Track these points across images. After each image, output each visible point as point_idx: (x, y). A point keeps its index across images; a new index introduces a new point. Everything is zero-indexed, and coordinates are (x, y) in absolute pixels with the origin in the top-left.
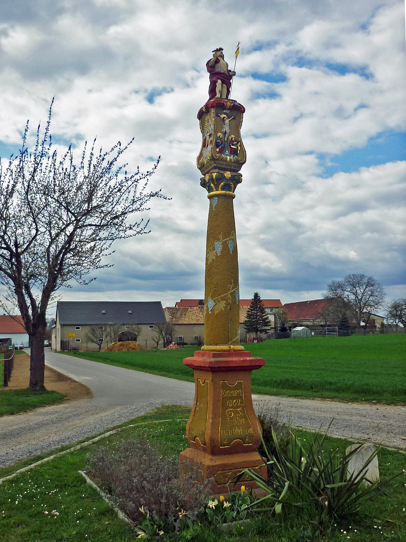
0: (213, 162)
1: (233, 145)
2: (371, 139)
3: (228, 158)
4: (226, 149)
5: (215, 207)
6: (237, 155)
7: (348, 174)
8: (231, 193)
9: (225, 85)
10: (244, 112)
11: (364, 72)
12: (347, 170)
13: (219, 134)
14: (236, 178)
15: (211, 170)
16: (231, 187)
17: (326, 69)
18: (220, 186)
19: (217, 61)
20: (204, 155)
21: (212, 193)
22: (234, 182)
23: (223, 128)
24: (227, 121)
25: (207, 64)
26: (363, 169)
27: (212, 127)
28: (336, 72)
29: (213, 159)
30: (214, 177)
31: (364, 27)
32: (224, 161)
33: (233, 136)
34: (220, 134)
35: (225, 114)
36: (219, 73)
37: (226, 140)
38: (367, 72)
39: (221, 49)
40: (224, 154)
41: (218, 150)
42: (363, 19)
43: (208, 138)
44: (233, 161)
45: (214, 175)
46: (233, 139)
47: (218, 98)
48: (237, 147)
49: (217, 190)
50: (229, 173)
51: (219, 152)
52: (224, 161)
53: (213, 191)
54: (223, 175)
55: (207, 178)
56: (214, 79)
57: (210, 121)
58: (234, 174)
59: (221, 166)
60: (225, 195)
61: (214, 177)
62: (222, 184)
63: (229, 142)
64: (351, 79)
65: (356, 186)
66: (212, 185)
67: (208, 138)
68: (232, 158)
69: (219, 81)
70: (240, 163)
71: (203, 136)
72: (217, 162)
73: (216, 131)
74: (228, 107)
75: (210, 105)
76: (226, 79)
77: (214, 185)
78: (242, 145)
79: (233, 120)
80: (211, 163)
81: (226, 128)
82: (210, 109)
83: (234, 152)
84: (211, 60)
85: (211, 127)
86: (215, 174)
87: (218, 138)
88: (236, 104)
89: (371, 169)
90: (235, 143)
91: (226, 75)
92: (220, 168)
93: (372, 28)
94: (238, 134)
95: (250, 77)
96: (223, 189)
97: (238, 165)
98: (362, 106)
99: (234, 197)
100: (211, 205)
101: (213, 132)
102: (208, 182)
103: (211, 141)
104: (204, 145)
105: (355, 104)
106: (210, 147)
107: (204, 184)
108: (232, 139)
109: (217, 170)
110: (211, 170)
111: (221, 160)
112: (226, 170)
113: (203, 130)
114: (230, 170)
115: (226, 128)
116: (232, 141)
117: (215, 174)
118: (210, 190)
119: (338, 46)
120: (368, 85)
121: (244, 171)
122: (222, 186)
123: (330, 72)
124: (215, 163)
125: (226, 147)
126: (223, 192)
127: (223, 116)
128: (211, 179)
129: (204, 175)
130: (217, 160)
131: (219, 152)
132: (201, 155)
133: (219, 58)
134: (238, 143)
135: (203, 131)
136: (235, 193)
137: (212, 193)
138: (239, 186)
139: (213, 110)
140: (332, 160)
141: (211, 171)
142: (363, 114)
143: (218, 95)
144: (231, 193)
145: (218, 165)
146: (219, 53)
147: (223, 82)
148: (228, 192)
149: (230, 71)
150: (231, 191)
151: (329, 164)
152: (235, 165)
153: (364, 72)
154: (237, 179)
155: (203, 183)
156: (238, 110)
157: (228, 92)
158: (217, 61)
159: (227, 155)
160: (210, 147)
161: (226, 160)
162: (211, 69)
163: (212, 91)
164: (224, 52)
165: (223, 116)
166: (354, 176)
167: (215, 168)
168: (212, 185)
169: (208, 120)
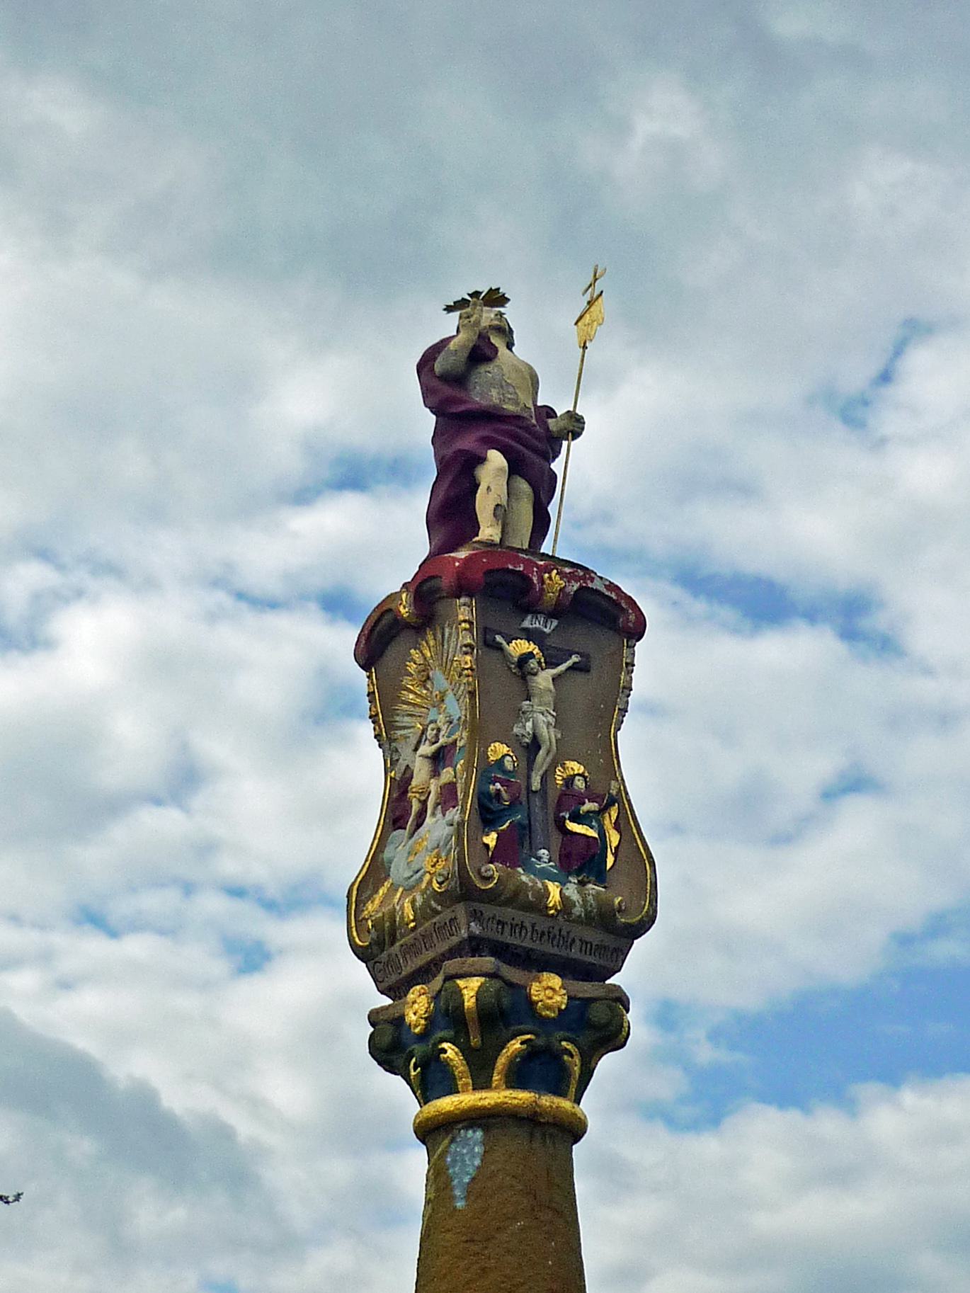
0: (461, 911)
1: (576, 818)
2: (905, 940)
3: (554, 890)
4: (539, 838)
5: (470, 1192)
6: (600, 876)
7: (793, 1116)
8: (566, 1104)
9: (523, 486)
10: (637, 630)
11: (852, 616)
12: (787, 1094)
13: (498, 750)
14: (598, 1013)
15: (453, 953)
16: (564, 1071)
17: (676, 592)
18: (502, 1061)
19: (481, 353)
20: (399, 870)
21: (447, 1104)
22: (587, 1037)
23: (519, 715)
24: (544, 679)
25: (425, 365)
26: (867, 1091)
27: (455, 708)
28: (727, 613)
29: (463, 890)
30: (469, 1002)
31: (852, 412)
32: (530, 907)
33: (575, 767)
34: (504, 749)
35: (530, 635)
36: (491, 416)
37: (536, 784)
38: (865, 623)
39: (496, 298)
40: (529, 869)
41: (491, 840)
42: (855, 374)
43: (421, 771)
44: (578, 910)
45: (470, 988)
46: (579, 784)
47: (490, 544)
48: (602, 833)
49: (482, 1084)
50: (556, 981)
51: (497, 855)
52: (530, 907)
53: (453, 1090)
54: (520, 991)
55: (417, 1006)
56: (467, 442)
57: (437, 674)
58: (587, 989)
59: (508, 939)
60: (529, 1120)
61: (469, 1002)
62: (515, 1045)
63: (553, 797)
64: (793, 654)
65: (841, 1175)
66: (451, 1052)
67: (421, 771)
68: (572, 891)
69: (496, 459)
70: (621, 929)
71: (391, 762)
72: (489, 910)
73: (480, 732)
74: (551, 596)
75: (446, 582)
76: (535, 450)
77: (466, 1051)
78: (627, 823)
79: (580, 678)
80: (447, 915)
81: (540, 720)
82: (441, 607)
83: (583, 860)
84: (444, 342)
85: (444, 707)
86: (476, 982)
87: (492, 770)
88: (597, 585)
89: (908, 1097)
90: (589, 806)
91: (528, 429)
92: (501, 951)
93: (889, 422)
94: (606, 760)
95: (313, 606)
96: (517, 1079)
97: (609, 940)
98: (854, 783)
99: (574, 1130)
100: (438, 1178)
101: (462, 737)
102: (423, 1037)
103: (448, 796)
104: (399, 813)
105: (821, 766)
106: (437, 827)
107: (390, 1046)
108: (569, 781)
109: (488, 962)
110: (453, 953)
111: (509, 902)
112: (538, 963)
113: (390, 726)
114: (566, 969)
115: (540, 720)
116: (569, 800)
117: (476, 982)
118: (431, 1081)
119: (743, 489)
120: (869, 681)
121: (636, 973)
122: (511, 1062)
123: (700, 606)
124: (475, 916)
125: (537, 826)
126: (522, 1097)
127: (520, 647)
128: (448, 1016)
129: (396, 990)
130: (492, 897)
131: (497, 855)
132: (375, 871)
133: (496, 341)
134: (604, 809)
135: (387, 737)
136: (590, 1105)
137: (447, 1104)
138: (607, 1064)
139: (464, 610)
140: (715, 1036)
141: (451, 966)
142: (858, 824)
143: (488, 531)
144: (566, 1104)
145: (493, 934)
146: (488, 316)
147: (516, 467)
148: (547, 1101)
149: (550, 412)
150: (562, 1093)
151: (706, 1054)
152: (595, 936)
153: (852, 616)
154: (601, 1028)
155: (386, 1039)
156: (602, 619)
157: (541, 523)
158: (481, 353)
159: (545, 875)
160: (437, 827)
161: (538, 905)
162: (448, 391)
163: (452, 513)
164: (510, 312)
165: (520, 647)
166: (828, 1124)
167: (474, 946)
168: (451, 1052)
169: (425, 669)
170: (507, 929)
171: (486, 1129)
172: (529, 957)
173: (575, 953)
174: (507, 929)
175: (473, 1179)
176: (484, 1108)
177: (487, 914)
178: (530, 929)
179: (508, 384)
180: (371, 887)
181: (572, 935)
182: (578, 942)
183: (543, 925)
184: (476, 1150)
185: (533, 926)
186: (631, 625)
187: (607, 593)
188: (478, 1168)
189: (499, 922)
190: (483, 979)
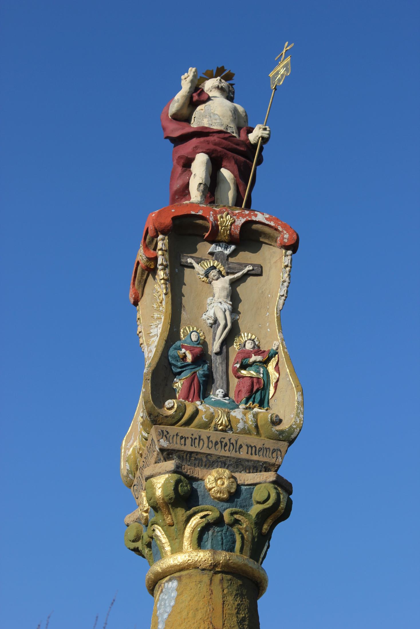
8: (168, 548)
49: (177, 549)
59: (189, 448)
62: (195, 521)
72: (173, 430)
109: (171, 465)
112: (211, 462)
124: (163, 434)
145: (177, 446)
167: (166, 454)
170: (188, 442)
171: (179, 579)
172: (249, 469)
173: (243, 454)
174: (188, 442)
175: (169, 615)
176: (176, 565)
177: (171, 433)
178: (206, 440)
179: (214, 114)
180: (133, 438)
181: (239, 443)
182: (245, 448)
183: (216, 436)
184: (173, 595)
185: (209, 438)
186: (286, 241)
187: (267, 222)
188: (173, 607)
189: (182, 438)
190: (167, 476)
